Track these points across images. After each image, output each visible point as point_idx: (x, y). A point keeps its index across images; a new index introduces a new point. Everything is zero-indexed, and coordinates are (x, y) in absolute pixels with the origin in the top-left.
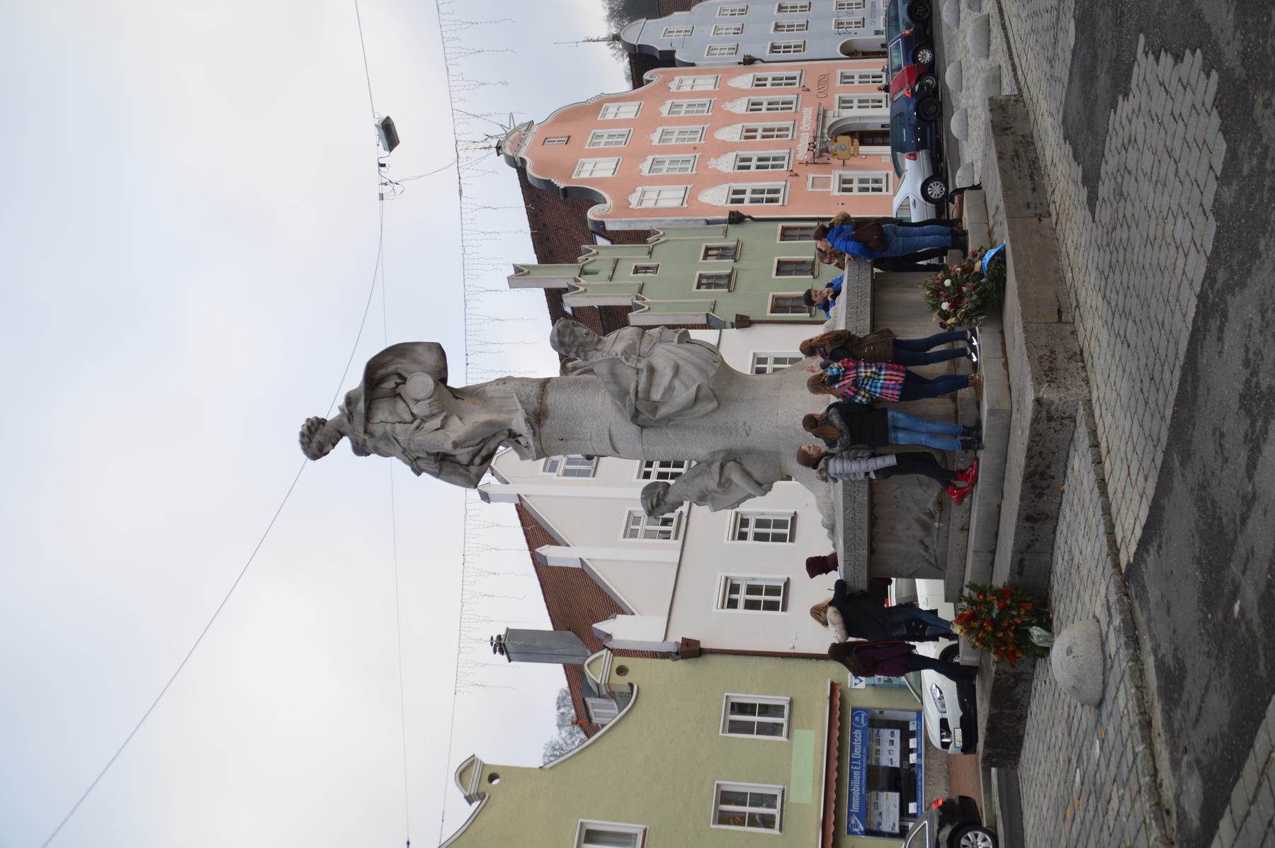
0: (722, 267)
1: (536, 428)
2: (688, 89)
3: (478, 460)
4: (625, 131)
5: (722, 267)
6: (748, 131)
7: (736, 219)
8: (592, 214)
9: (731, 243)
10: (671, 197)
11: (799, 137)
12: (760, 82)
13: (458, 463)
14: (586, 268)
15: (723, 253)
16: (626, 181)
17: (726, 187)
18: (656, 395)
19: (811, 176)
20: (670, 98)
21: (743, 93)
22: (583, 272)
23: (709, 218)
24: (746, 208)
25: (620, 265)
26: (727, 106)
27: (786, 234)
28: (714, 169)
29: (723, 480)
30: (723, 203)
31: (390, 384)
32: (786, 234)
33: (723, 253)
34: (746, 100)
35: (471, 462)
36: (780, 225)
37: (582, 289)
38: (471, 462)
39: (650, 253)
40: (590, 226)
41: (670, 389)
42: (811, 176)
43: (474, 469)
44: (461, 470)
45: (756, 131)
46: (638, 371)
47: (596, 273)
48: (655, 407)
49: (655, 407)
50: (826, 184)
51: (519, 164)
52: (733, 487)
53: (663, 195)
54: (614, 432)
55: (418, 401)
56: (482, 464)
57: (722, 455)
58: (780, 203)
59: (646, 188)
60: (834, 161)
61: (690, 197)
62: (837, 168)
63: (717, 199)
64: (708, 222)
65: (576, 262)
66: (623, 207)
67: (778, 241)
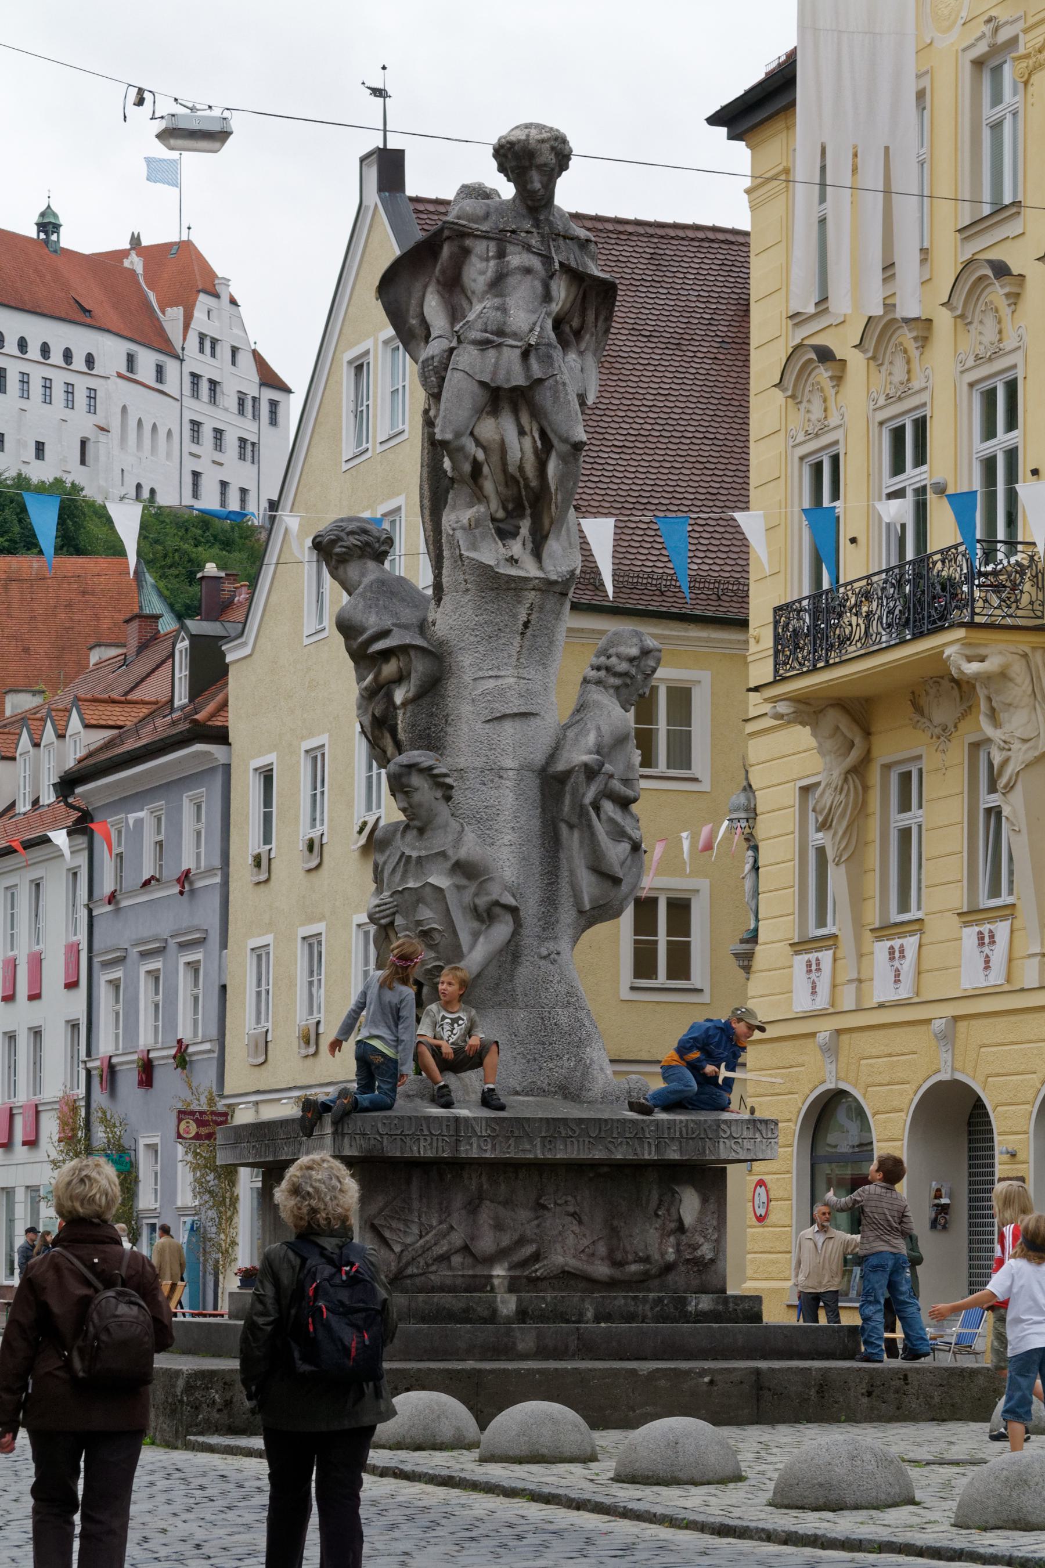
52: (476, 925)
54: (535, 722)
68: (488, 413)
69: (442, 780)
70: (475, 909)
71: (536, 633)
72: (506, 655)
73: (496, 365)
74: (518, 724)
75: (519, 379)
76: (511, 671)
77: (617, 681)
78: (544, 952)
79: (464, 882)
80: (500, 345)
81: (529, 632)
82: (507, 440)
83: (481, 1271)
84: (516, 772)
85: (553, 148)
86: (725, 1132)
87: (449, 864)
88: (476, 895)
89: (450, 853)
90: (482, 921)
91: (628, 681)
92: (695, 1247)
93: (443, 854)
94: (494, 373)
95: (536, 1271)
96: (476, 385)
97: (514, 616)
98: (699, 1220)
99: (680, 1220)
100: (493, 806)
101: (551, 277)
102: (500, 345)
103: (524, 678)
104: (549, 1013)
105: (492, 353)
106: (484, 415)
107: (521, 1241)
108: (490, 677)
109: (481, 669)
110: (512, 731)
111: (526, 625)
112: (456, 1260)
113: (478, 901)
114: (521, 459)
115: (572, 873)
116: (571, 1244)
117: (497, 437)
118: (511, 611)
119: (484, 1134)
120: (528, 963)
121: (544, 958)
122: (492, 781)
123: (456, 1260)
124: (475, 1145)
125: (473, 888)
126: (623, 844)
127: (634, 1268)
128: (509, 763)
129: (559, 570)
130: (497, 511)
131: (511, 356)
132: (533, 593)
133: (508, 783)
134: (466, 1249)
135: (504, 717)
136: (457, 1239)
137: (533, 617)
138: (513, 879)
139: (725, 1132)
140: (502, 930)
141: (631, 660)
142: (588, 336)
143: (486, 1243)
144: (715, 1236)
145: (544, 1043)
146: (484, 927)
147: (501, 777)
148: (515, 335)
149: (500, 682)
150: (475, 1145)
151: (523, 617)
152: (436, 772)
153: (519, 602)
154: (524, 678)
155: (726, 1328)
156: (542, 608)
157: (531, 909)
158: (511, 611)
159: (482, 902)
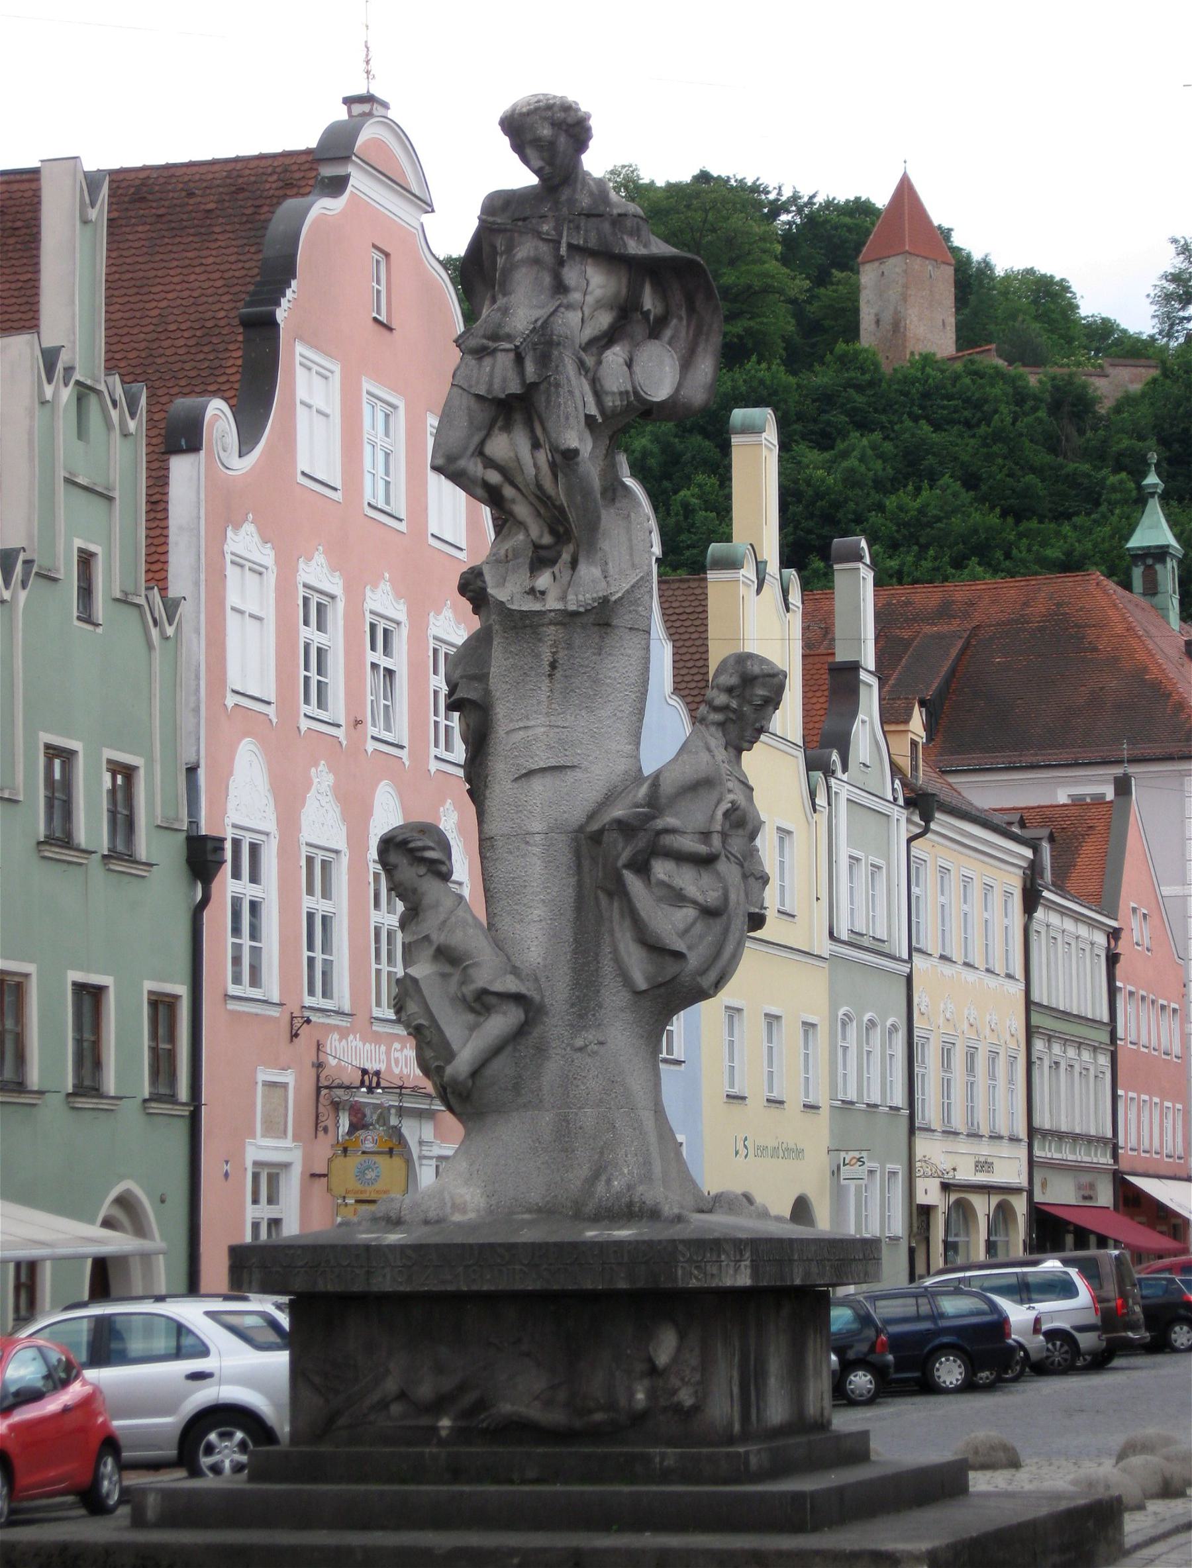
0: (91, 826)
1: (591, 618)
2: (233, 598)
3: (494, 477)
4: (400, 506)
5: (91, 826)
6: (254, 849)
7: (202, 857)
8: (218, 414)
9: (143, 847)
10: (250, 662)
11: (377, 1038)
12: (318, 871)
13: (488, 435)
14: (93, 400)
15: (122, 819)
16: (290, 516)
17: (270, 825)
18: (661, 869)
19: (288, 1077)
20: (347, 589)
21: (289, 818)
22: (84, 391)
23: (201, 772)
24: (228, 886)
25: (99, 504)
26: (322, 779)
27: (162, 1005)
28: (308, 784)
29: (493, 1000)
30: (234, 815)
31: (649, 301)
32: (162, 1005)
33: (122, 819)
34: (340, 843)
35: (490, 463)
36: (182, 990)
37: (49, 391)
38: (490, 463)
39: (124, 601)
40: (183, 403)
41: (678, 898)
42: (288, 1077)
43: (475, 468)
44: (476, 439)
45: (326, 894)
46: (706, 836)
47: (82, 431)
48: (641, 867)
49: (641, 867)
50: (274, 1128)
51: (327, 171)
52: (471, 1017)
53: (251, 624)
54: (570, 776)
55: (629, 364)
56: (486, 485)
57: (537, 998)
58: (233, 990)
59: (271, 578)
60: (324, 1148)
61: (247, 718)
62: (307, 1158)
63: (243, 803)
64: (192, 770)
65: (109, 370)
66: (226, 509)
67: (149, 985)
68: (501, 429)
69: (419, 854)
70: (464, 999)
71: (567, 673)
72: (535, 702)
73: (491, 375)
74: (548, 780)
75: (515, 387)
76: (542, 719)
77: (718, 717)
78: (579, 1042)
79: (448, 969)
80: (495, 350)
81: (558, 674)
82: (520, 455)
83: (425, 1421)
84: (543, 836)
85: (545, 119)
86: (684, 1255)
87: (431, 951)
88: (463, 983)
89: (434, 937)
90: (478, 1013)
91: (732, 716)
92: (675, 1392)
93: (427, 938)
94: (490, 384)
95: (483, 1420)
96: (473, 401)
97: (538, 656)
98: (675, 1360)
99: (650, 1360)
100: (519, 877)
101: (561, 262)
102: (495, 350)
103: (558, 727)
104: (576, 1114)
105: (487, 361)
106: (496, 431)
107: (462, 1388)
108: (520, 729)
109: (512, 721)
110: (541, 788)
111: (553, 665)
112: (396, 1409)
113: (465, 990)
114: (536, 476)
115: (615, 951)
116: (524, 1392)
117: (512, 454)
118: (533, 651)
119: (399, 1264)
120: (558, 1057)
121: (580, 1049)
122: (518, 848)
123: (396, 1409)
124: (388, 1277)
125: (456, 978)
126: (685, 910)
127: (599, 1417)
128: (537, 826)
129: (581, 598)
130: (541, 536)
131: (504, 361)
132: (552, 627)
133: (536, 850)
134: (402, 1396)
135: (530, 773)
136: (391, 1385)
137: (560, 655)
138: (539, 960)
139: (684, 1255)
140: (499, 1023)
141: (730, 690)
142: (674, 322)
143: (425, 1390)
144: (697, 1377)
145: (566, 1151)
146: (482, 1019)
147: (527, 843)
148: (509, 338)
149: (530, 732)
150: (388, 1277)
151: (547, 657)
152: (412, 845)
153: (540, 640)
154: (558, 727)
155: (462, 1493)
156: (569, 646)
157: (557, 994)
158: (533, 651)
159: (469, 990)
